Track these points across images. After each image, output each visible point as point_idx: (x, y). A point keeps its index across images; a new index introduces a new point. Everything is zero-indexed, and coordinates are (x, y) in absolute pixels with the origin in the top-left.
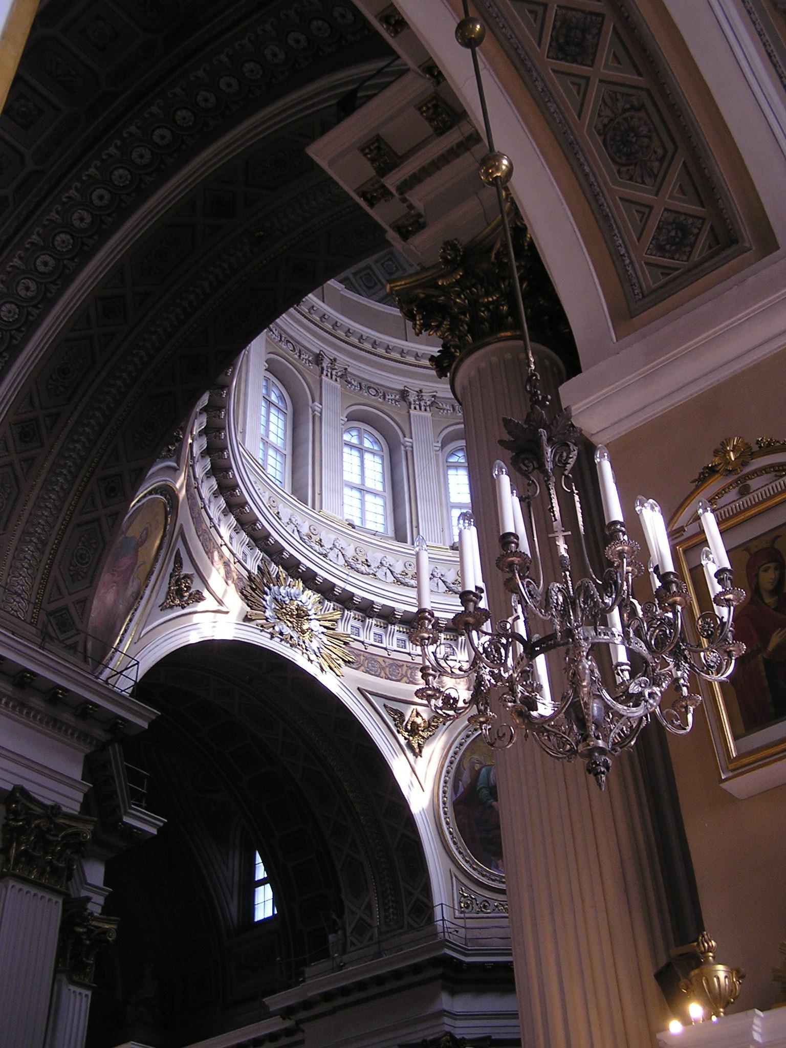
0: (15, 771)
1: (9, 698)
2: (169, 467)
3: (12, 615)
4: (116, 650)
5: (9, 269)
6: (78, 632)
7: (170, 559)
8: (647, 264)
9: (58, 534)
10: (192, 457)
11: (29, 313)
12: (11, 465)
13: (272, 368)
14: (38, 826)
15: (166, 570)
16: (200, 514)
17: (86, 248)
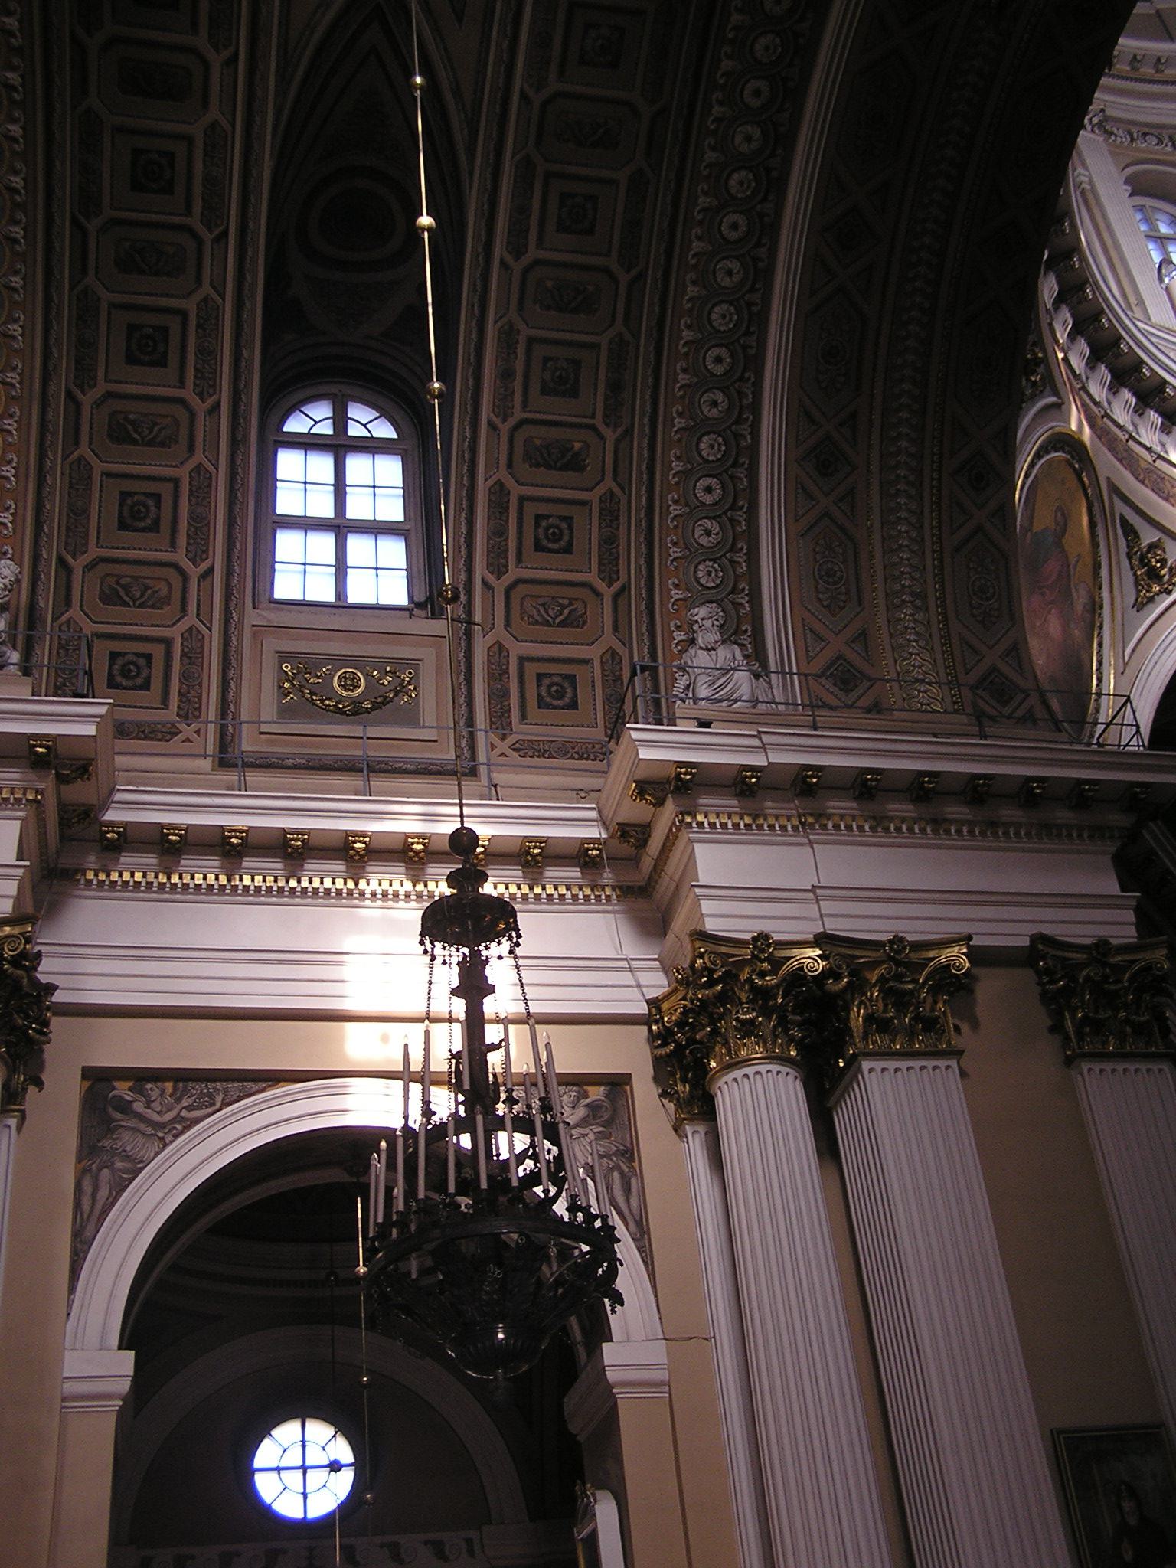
1: (971, 824)
2: (1048, 408)
3: (926, 711)
4: (1099, 694)
5: (693, 262)
6: (873, 681)
7: (1116, 534)
9: (935, 575)
10: (1077, 377)
11: (749, 304)
12: (826, 514)
13: (1140, 187)
14: (1088, 978)
15: (1117, 550)
16: (1129, 450)
17: (775, 174)
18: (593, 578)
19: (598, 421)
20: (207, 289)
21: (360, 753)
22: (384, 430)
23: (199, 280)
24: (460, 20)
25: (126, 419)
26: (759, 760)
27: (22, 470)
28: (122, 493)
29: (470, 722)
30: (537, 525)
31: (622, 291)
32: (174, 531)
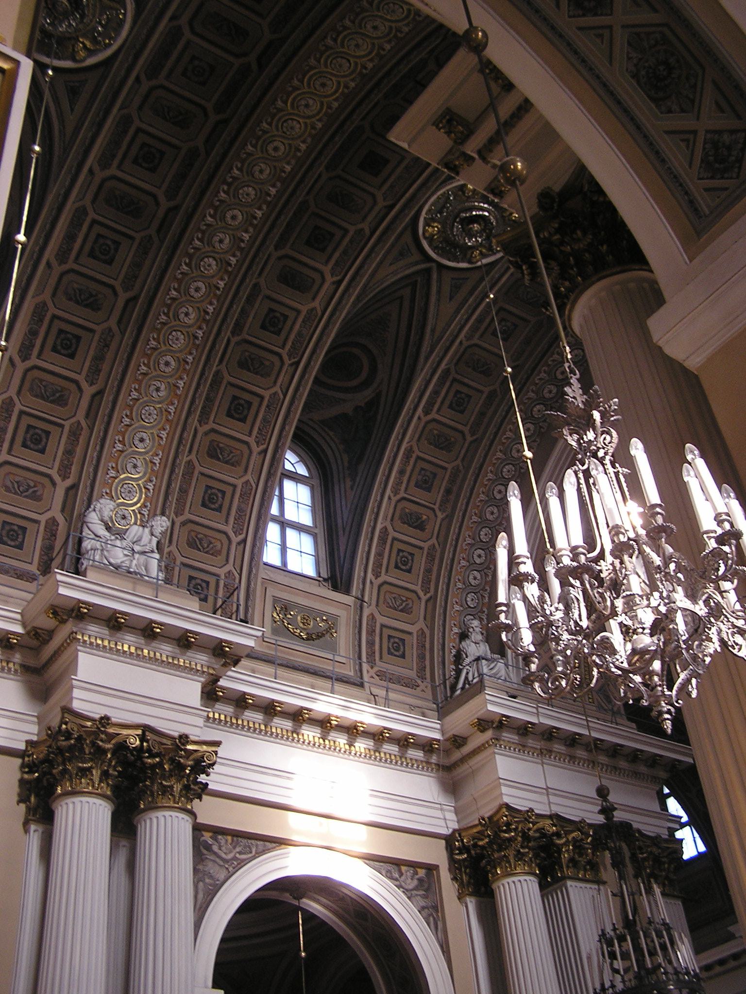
0: (584, 808)
8: (706, 190)
18: (418, 589)
19: (436, 507)
20: (277, 389)
21: (274, 653)
22: (302, 470)
23: (275, 383)
24: (451, 299)
25: (218, 446)
26: (534, 720)
27: (164, 461)
28: (207, 486)
29: (360, 658)
30: (398, 555)
31: (466, 445)
32: (228, 514)
